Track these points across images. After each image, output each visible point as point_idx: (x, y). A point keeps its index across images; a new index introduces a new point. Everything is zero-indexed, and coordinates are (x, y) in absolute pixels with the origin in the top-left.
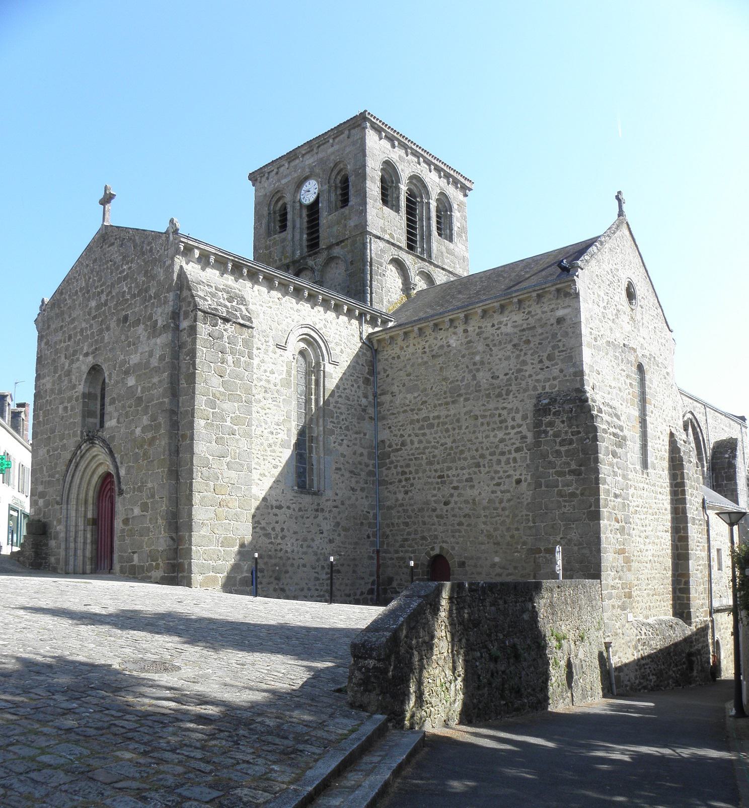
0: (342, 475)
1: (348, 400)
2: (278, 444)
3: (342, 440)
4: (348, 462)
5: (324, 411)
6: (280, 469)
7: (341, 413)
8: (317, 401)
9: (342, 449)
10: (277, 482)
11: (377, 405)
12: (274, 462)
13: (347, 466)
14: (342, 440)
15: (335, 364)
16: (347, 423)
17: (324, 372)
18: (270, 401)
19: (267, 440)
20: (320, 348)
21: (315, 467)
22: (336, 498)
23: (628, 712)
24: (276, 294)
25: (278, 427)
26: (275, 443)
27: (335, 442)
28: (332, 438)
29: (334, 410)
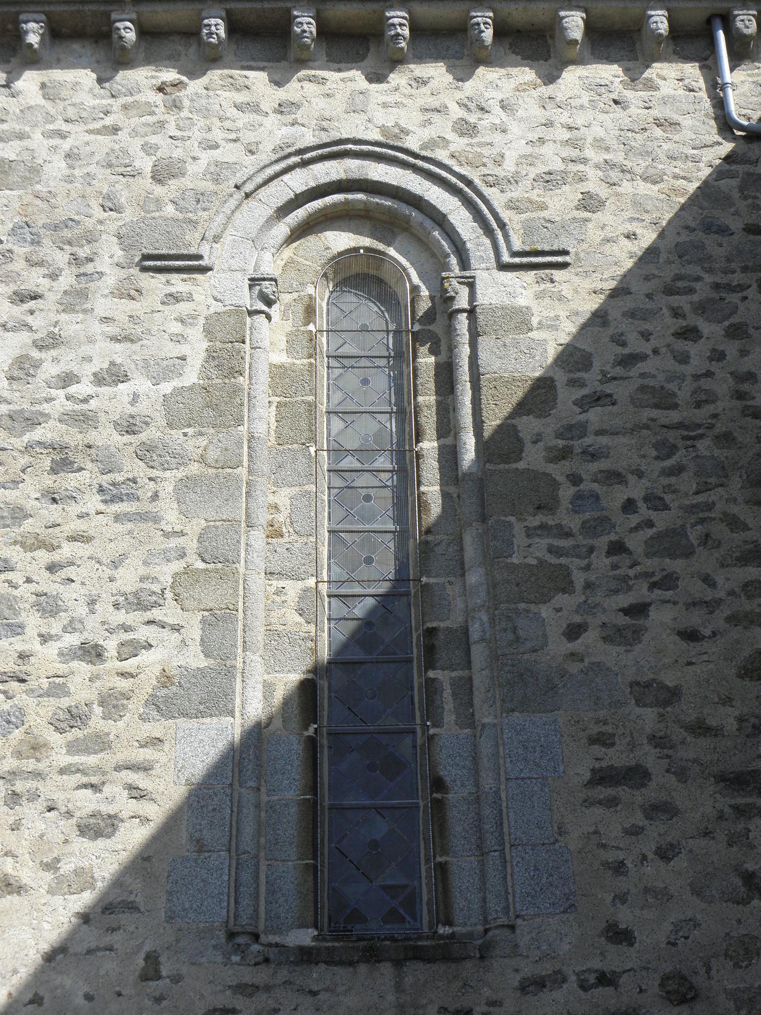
0: (661, 810)
1: (665, 401)
2: (136, 706)
3: (638, 610)
4: (701, 729)
5: (507, 479)
6: (133, 837)
7: (615, 477)
8: (449, 455)
9: (658, 651)
10: (110, 910)
11: (679, 378)
12: (87, 803)
13: (695, 749)
14: (638, 610)
15: (543, 261)
16: (662, 521)
17: (472, 312)
18: (93, 502)
19: (57, 689)
20: (440, 220)
21: (456, 795)
22: (616, 959)
23: (422, 779)
24: (141, 79)
25: (133, 618)
26: (112, 704)
27: (574, 632)
28: (554, 613)
29: (559, 471)
